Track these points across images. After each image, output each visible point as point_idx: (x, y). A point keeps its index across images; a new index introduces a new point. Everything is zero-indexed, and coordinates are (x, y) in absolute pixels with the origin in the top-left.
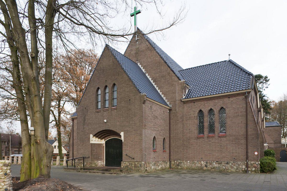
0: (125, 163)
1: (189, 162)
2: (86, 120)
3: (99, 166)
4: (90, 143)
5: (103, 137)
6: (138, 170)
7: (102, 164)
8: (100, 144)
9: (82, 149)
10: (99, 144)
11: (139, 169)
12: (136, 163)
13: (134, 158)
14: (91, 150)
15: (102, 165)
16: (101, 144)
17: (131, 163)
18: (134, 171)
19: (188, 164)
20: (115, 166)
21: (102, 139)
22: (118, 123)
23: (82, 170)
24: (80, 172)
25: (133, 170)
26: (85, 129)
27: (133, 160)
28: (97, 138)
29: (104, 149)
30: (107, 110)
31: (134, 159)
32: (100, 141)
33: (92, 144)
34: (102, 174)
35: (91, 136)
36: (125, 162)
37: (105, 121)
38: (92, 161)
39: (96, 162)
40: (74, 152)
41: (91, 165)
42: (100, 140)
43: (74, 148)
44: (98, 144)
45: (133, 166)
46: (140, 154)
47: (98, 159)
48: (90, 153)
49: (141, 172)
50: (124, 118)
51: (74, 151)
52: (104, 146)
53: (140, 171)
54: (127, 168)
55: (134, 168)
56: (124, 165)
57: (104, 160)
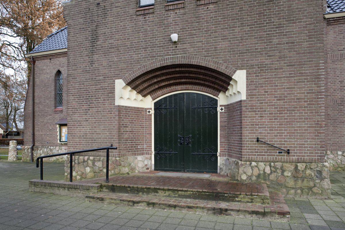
0: (256, 166)
1: (340, 153)
2: (101, 39)
3: (139, 172)
4: (116, 104)
5: (153, 88)
6: (310, 188)
7: (146, 165)
8: (141, 108)
9: (84, 123)
10: (138, 108)
11: (311, 184)
12: (301, 166)
13: (288, 150)
14: (116, 127)
15: (148, 169)
16: (143, 108)
17: (279, 165)
18: (292, 191)
19: (340, 157)
20: (188, 171)
21: (145, 96)
22: (223, 45)
23: (104, 189)
24: (106, 202)
25: (286, 187)
26: (96, 65)
27: (285, 157)
28: (135, 92)
29: (151, 124)
30: (180, 6)
31: (289, 153)
32: (142, 100)
33: (120, 108)
34: (214, 213)
35: (119, 84)
36: (254, 164)
37: (175, 37)
38: (122, 158)
39: (131, 158)
40: (35, 131)
41: (120, 170)
42: (140, 97)
43: (36, 122)
44: (135, 108)
45: (287, 174)
46: (312, 139)
47: (136, 151)
48: (115, 132)
49: (321, 194)
50: (247, 28)
51: (36, 129)
52: (151, 115)
53: (315, 190)
54: (265, 180)
55: (291, 183)
56: (249, 172)
57: (151, 154)
